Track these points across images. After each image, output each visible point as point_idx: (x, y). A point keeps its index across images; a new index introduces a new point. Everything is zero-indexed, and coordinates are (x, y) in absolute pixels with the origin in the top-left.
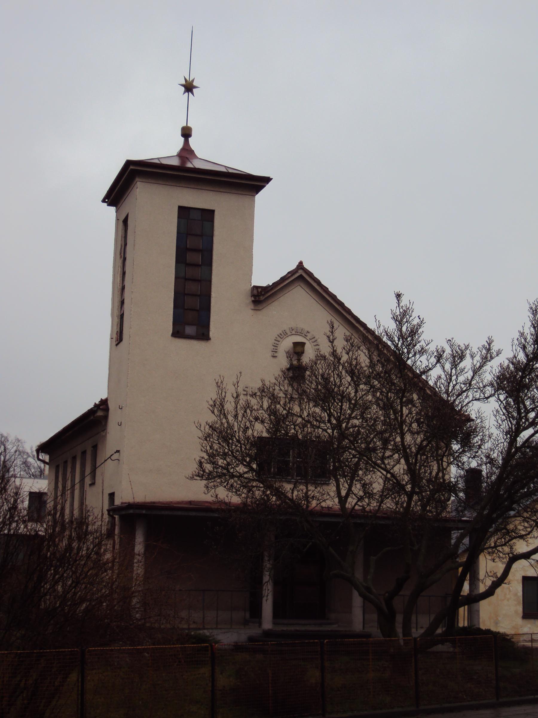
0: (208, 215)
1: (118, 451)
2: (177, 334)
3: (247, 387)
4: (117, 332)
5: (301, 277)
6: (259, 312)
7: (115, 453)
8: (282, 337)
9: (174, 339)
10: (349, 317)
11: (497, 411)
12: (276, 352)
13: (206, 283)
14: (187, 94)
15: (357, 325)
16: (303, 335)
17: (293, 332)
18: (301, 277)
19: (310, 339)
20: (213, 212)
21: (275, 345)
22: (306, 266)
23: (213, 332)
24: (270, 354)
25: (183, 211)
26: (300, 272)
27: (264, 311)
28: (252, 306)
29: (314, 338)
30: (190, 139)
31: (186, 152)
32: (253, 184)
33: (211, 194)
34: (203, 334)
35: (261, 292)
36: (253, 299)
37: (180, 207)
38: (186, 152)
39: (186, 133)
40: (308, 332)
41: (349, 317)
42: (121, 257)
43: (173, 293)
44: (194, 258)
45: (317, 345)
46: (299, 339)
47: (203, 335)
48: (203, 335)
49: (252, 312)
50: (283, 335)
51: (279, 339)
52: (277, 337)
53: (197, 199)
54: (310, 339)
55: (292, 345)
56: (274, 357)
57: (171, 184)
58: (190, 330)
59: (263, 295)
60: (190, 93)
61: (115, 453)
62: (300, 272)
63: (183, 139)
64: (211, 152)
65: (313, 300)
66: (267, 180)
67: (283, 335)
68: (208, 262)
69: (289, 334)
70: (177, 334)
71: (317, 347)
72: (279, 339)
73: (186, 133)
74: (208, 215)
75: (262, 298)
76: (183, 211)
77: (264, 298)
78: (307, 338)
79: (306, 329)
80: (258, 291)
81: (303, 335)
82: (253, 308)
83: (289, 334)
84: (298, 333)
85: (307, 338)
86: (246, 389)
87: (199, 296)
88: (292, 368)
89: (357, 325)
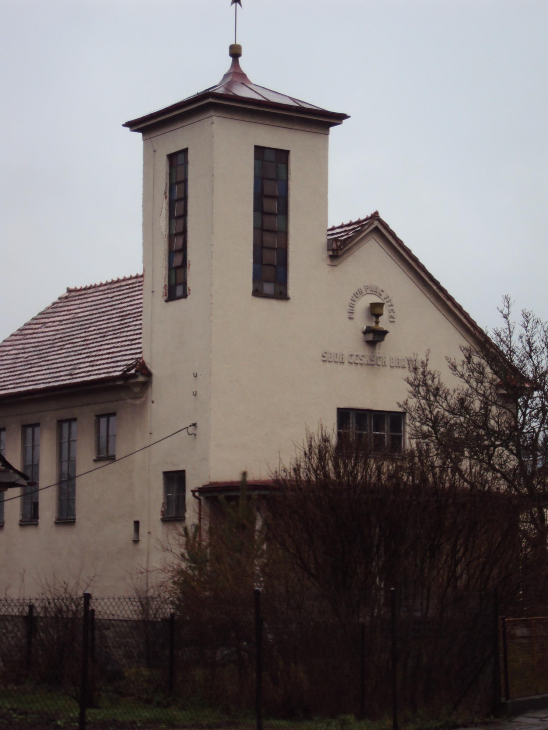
0: (283, 156)
1: (194, 425)
2: (257, 293)
3: (326, 353)
4: (166, 285)
5: (376, 229)
6: (335, 268)
7: (190, 426)
8: (357, 296)
9: (254, 298)
10: (423, 274)
11: (464, 362)
12: (352, 313)
13: (283, 234)
14: (234, 4)
15: (430, 283)
16: (378, 294)
17: (369, 291)
18: (374, 228)
19: (385, 299)
20: (287, 152)
21: (351, 305)
22: (382, 216)
23: (291, 291)
24: (346, 315)
25: (259, 150)
26: (376, 223)
27: (340, 267)
28: (328, 261)
29: (388, 297)
30: (240, 59)
31: (236, 74)
32: (321, 121)
33: (286, 131)
34: (281, 293)
35: (340, 246)
36: (331, 253)
37: (256, 147)
38: (236, 74)
39: (235, 52)
40: (382, 291)
41: (423, 274)
42: (166, 197)
43: (252, 247)
44: (272, 205)
45: (392, 305)
46: (376, 299)
47: (282, 295)
48: (282, 295)
49: (328, 268)
50: (358, 294)
51: (355, 298)
52: (353, 296)
53: (273, 137)
54: (385, 299)
55: (369, 305)
56: (351, 318)
57: (279, 124)
58: (268, 288)
59: (341, 249)
60: (238, 4)
61: (190, 426)
62: (376, 223)
63: (231, 59)
64: (272, 77)
65: (387, 255)
66: (348, 117)
67: (358, 294)
68: (284, 211)
69: (365, 293)
70: (257, 293)
71: (391, 308)
72: (355, 298)
73: (235, 52)
74: (283, 156)
75: (340, 252)
76: (259, 150)
77: (342, 252)
78: (381, 297)
79: (381, 287)
80: (337, 245)
81: (378, 294)
82: (329, 263)
83: (365, 293)
84: (374, 291)
85: (381, 297)
86: (325, 355)
87: (276, 249)
88: (368, 331)
89: (430, 283)
